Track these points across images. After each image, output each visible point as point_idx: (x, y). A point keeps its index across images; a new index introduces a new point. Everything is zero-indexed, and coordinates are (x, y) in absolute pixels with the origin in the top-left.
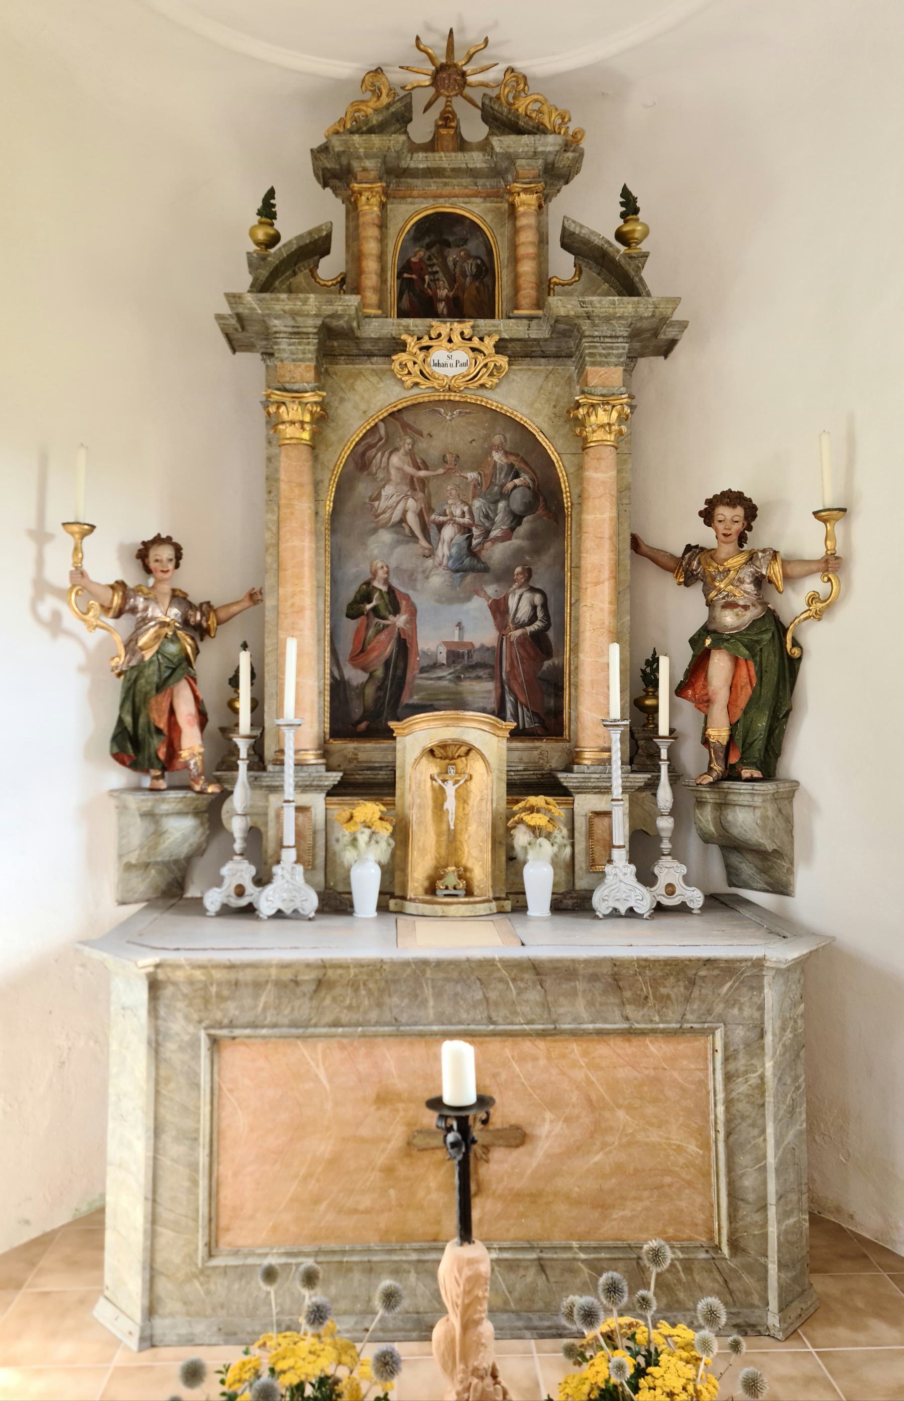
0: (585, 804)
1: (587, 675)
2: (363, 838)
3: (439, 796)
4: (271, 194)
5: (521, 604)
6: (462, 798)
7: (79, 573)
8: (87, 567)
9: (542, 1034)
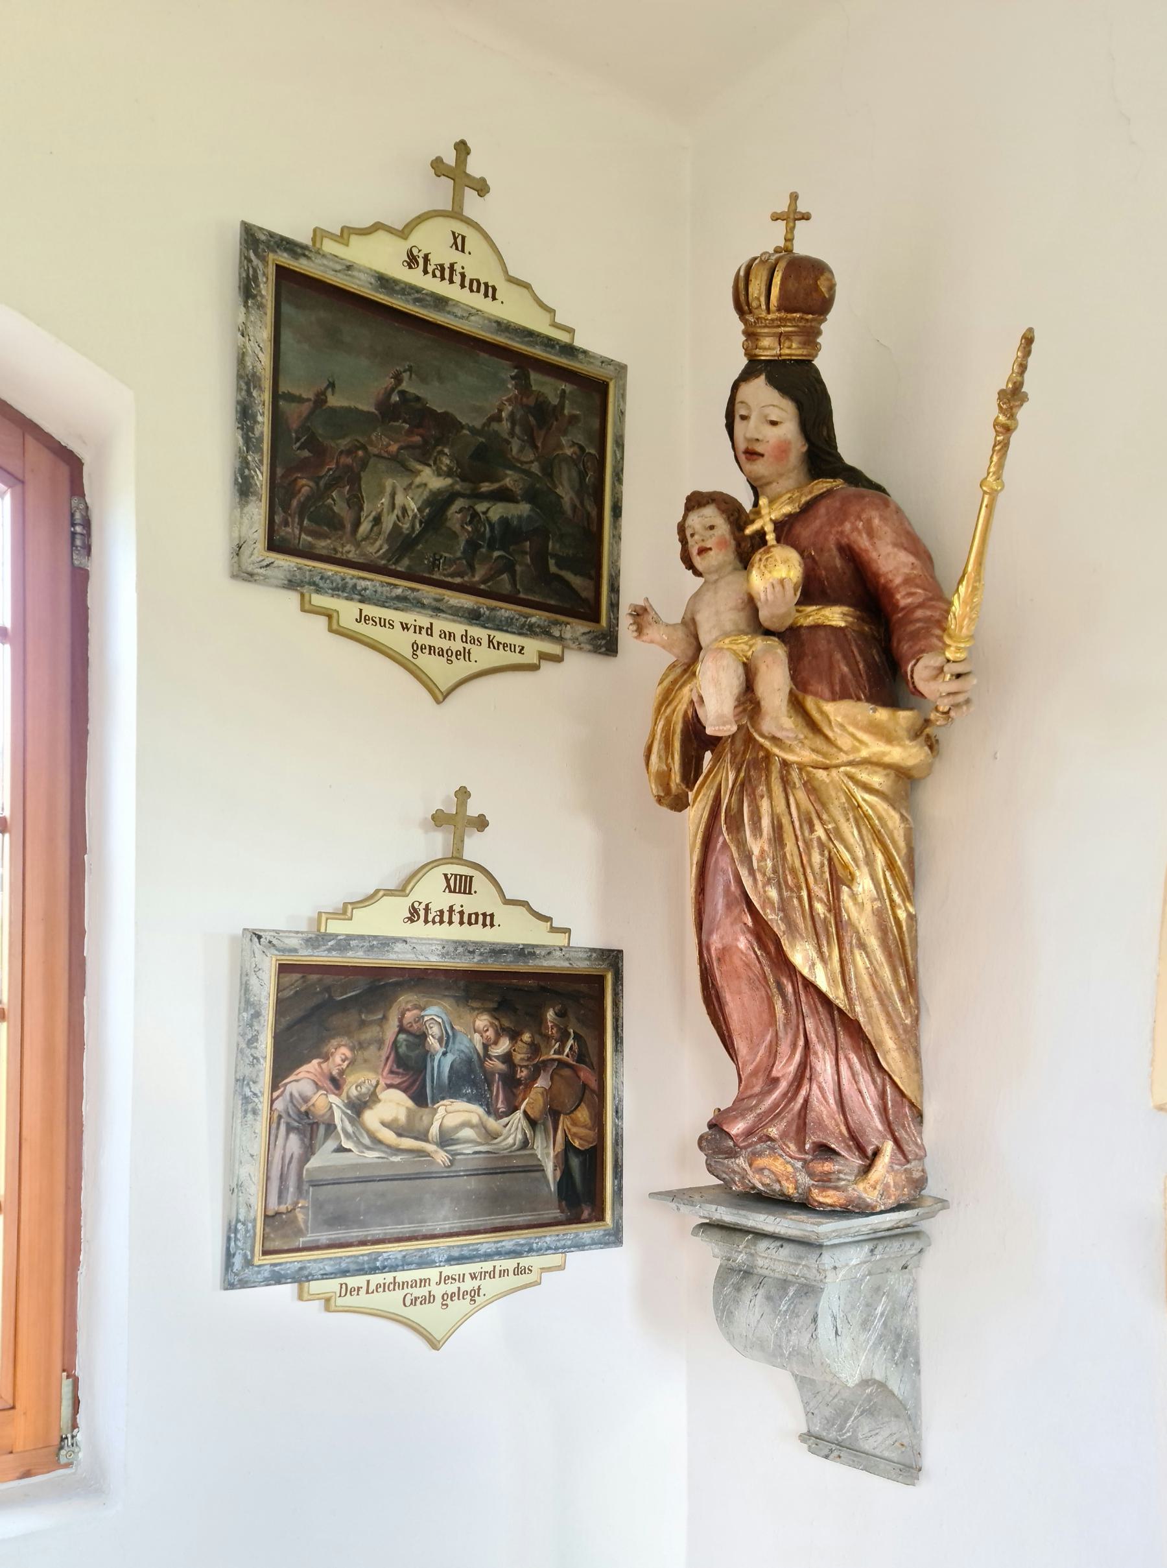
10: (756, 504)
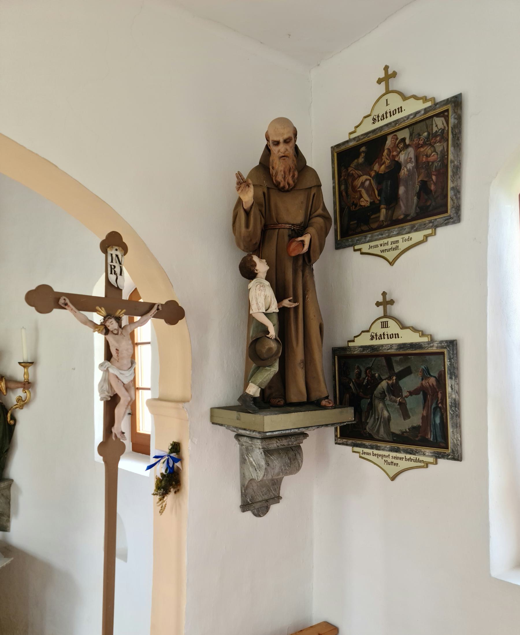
10: (382, 411)
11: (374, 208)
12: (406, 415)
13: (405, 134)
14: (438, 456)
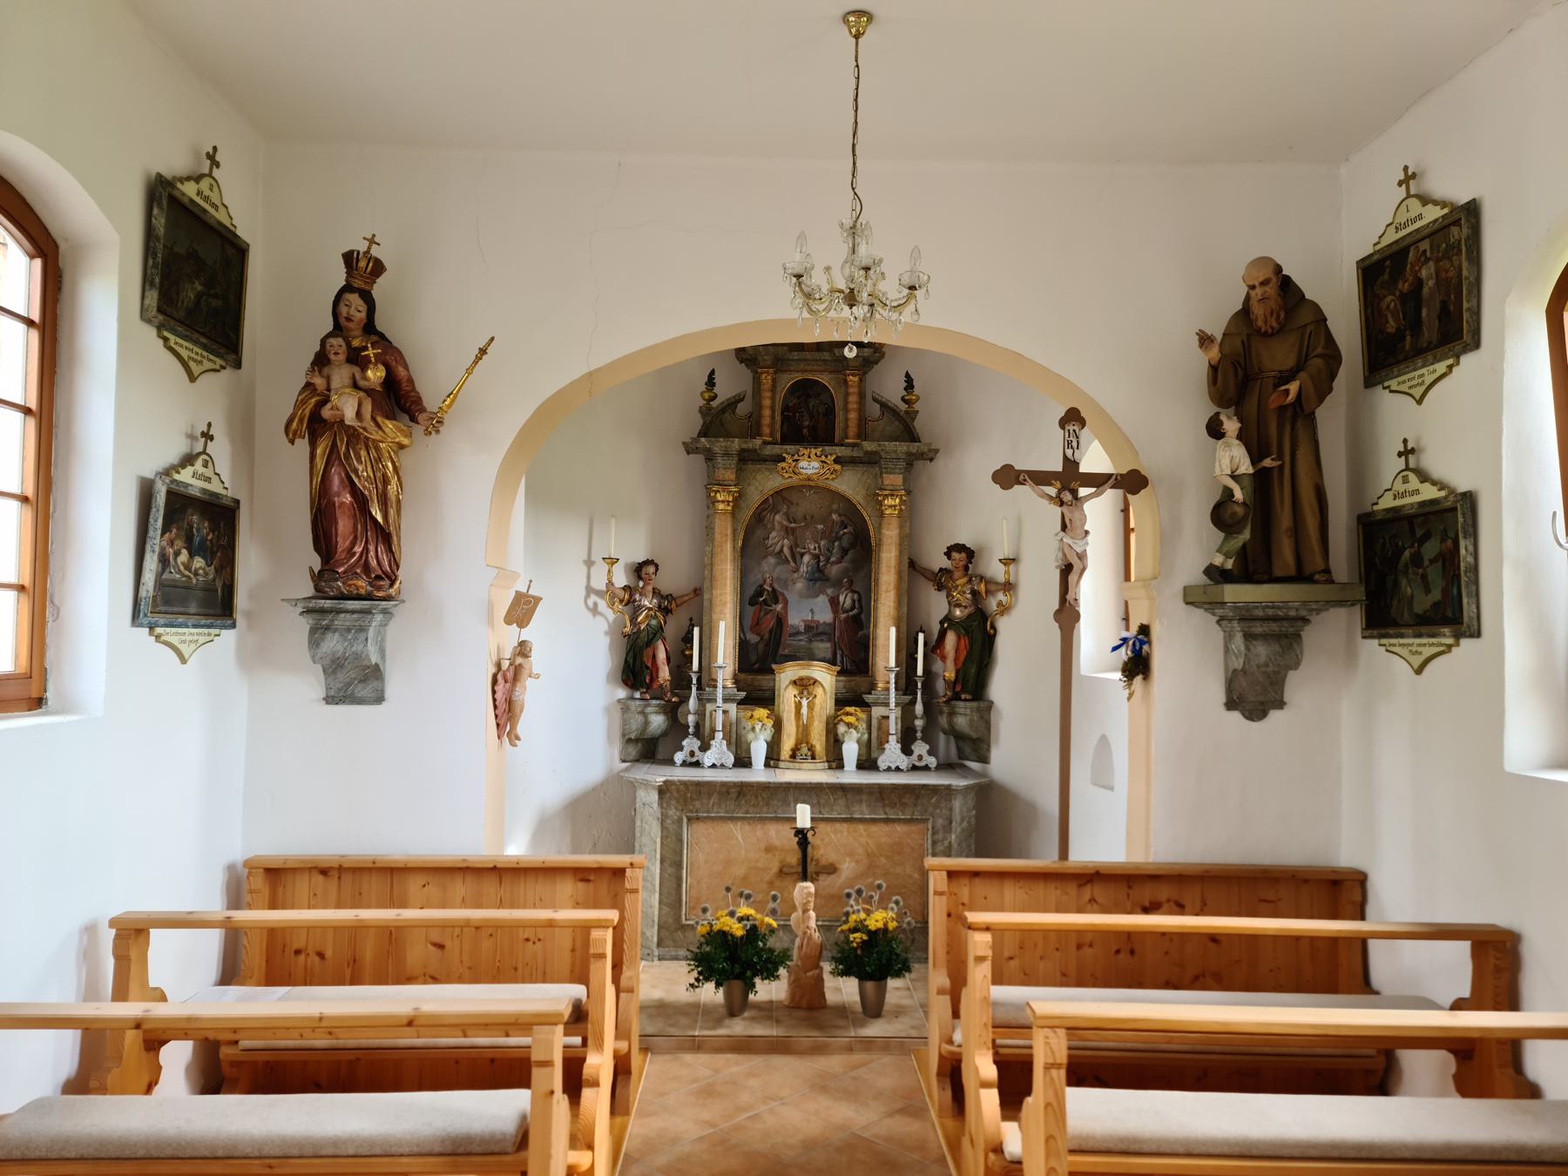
0: (877, 712)
1: (880, 642)
2: (758, 727)
3: (798, 706)
4: (713, 372)
5: (846, 599)
6: (811, 707)
7: (610, 583)
8: (614, 580)
9: (846, 820)
11: (1399, 336)
12: (1427, 590)
13: (1425, 245)
14: (1458, 636)
